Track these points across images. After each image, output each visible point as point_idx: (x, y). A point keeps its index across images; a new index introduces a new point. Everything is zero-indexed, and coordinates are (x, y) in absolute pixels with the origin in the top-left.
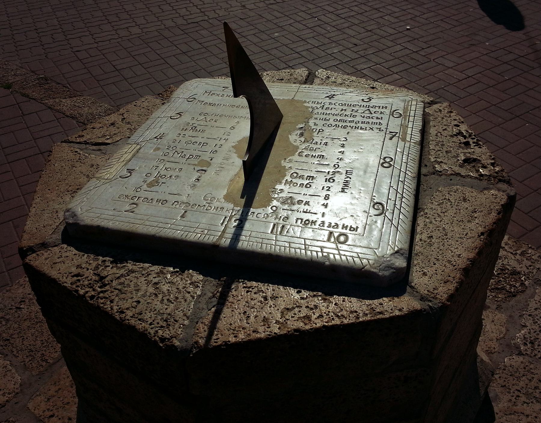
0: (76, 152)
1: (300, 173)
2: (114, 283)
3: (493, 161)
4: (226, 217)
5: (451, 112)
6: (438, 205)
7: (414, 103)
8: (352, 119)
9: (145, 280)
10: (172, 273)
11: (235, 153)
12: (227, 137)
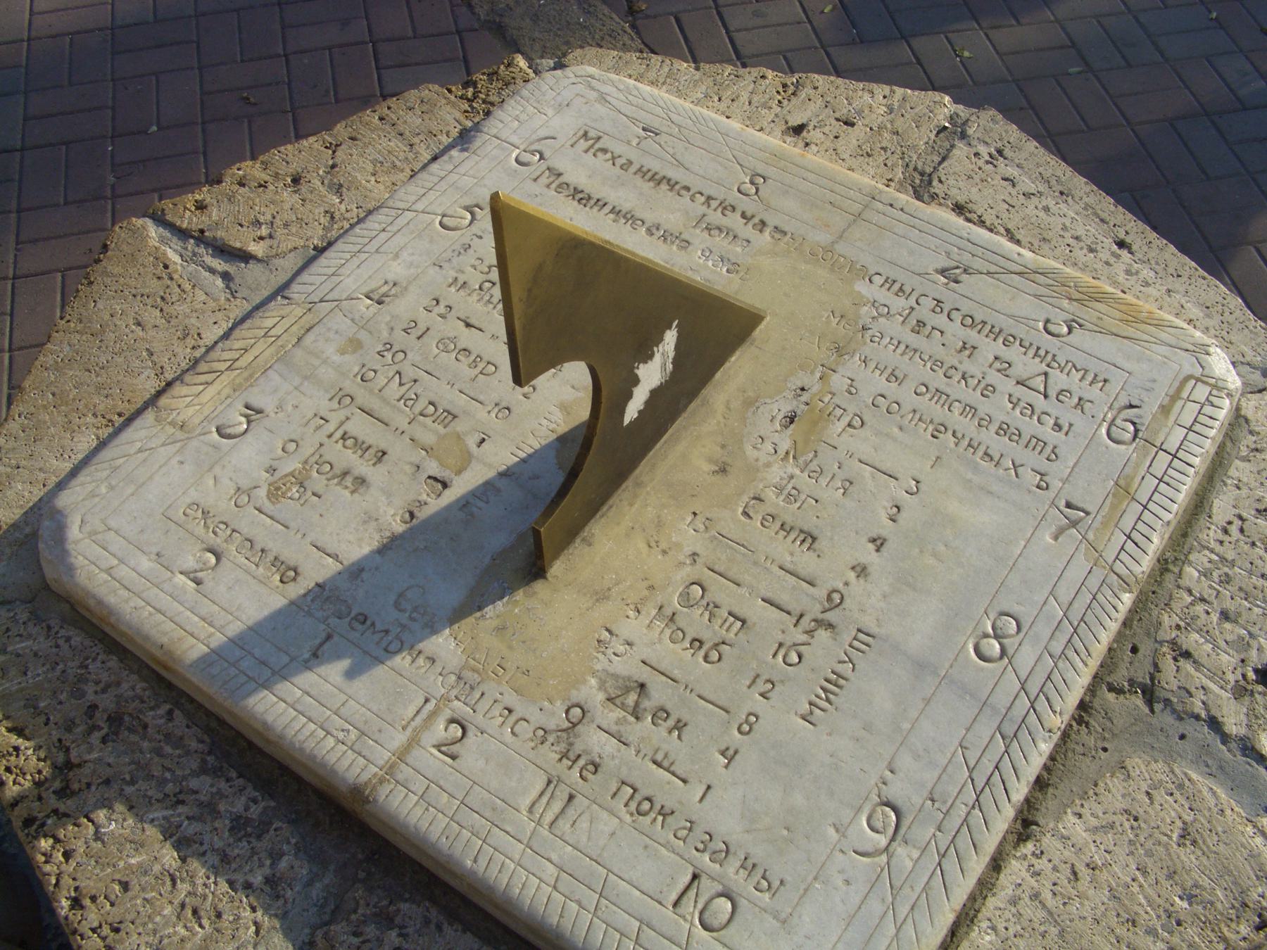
1: (720, 591)
8: (974, 397)
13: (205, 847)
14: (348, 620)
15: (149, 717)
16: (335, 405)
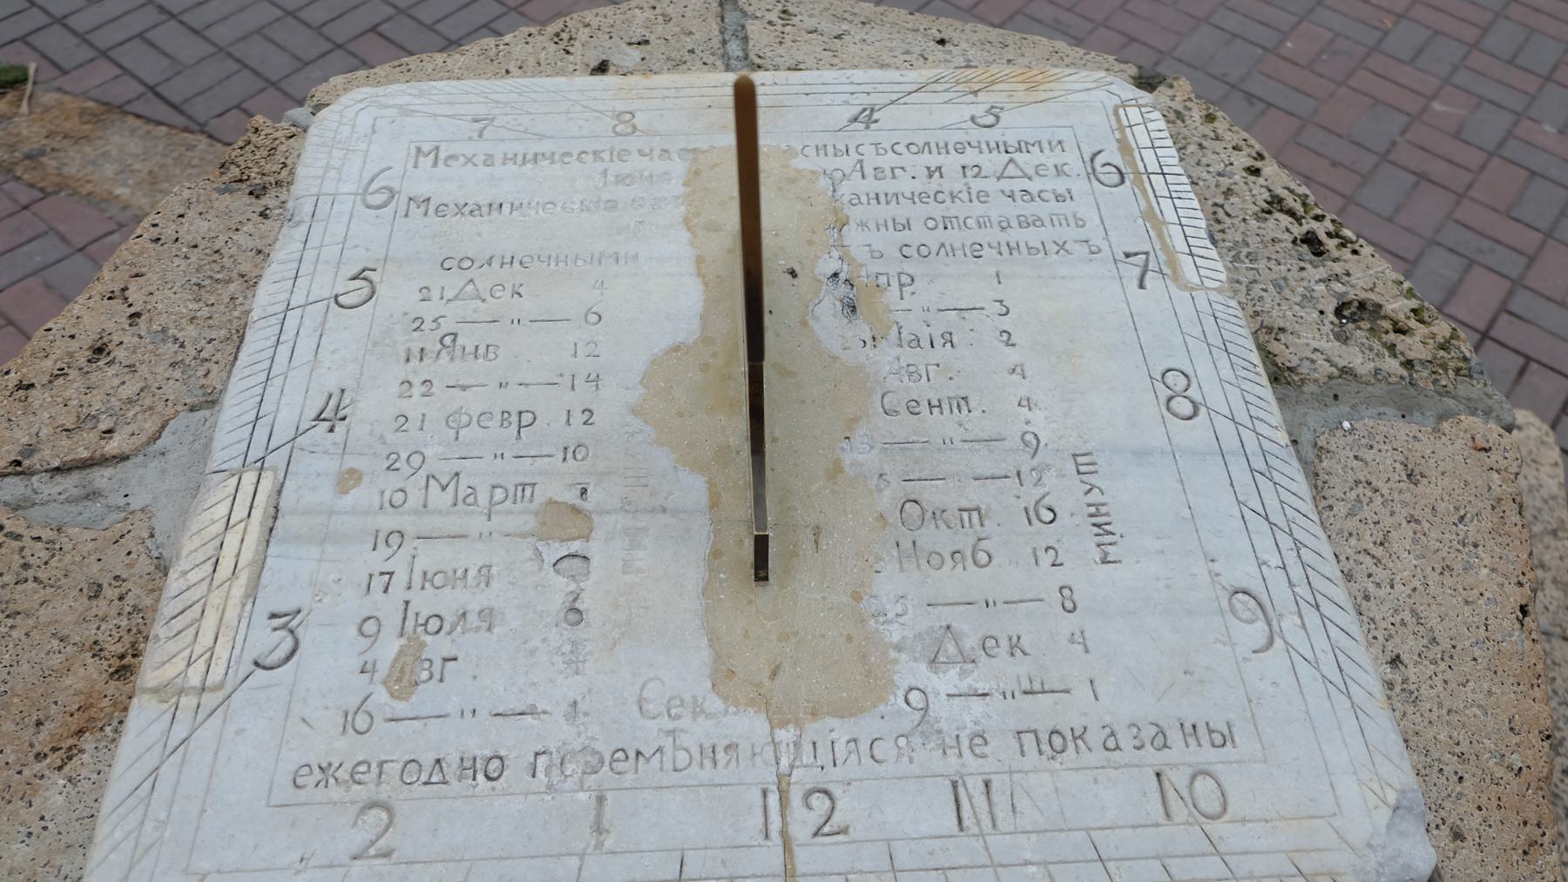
1: (932, 495)
3: (1414, 303)
4: (765, 793)
5: (1210, 118)
6: (1351, 514)
7: (1134, 113)
8: (978, 209)
14: (606, 768)
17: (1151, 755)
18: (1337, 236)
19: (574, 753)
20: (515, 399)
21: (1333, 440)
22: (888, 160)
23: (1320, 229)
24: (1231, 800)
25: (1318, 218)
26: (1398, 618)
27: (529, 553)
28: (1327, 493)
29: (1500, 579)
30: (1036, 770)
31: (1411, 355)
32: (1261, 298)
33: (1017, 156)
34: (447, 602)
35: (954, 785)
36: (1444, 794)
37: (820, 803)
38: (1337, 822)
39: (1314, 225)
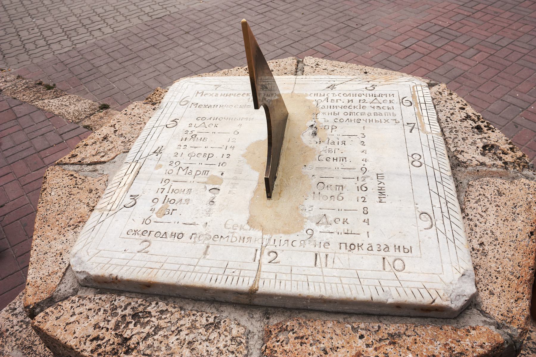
0: (72, 175)
1: (327, 182)
2: (142, 346)
3: (511, 146)
4: (257, 250)
5: (451, 94)
6: (476, 202)
7: (419, 88)
8: (362, 110)
9: (177, 339)
10: (207, 325)
11: (248, 163)
12: (232, 144)
13: (199, 342)
15: (149, 309)
16: (163, 183)
17: (382, 253)
18: (488, 127)
19: (203, 235)
20: (208, 151)
21: (474, 183)
22: (335, 98)
23: (482, 125)
24: (406, 267)
25: (482, 122)
26: (485, 232)
27: (203, 187)
28: (469, 197)
29: (524, 224)
30: (344, 253)
31: (507, 160)
32: (457, 142)
33: (378, 98)
34: (177, 197)
35: (316, 255)
36: (490, 281)
37: (273, 255)
38: (441, 276)
39: (480, 124)
